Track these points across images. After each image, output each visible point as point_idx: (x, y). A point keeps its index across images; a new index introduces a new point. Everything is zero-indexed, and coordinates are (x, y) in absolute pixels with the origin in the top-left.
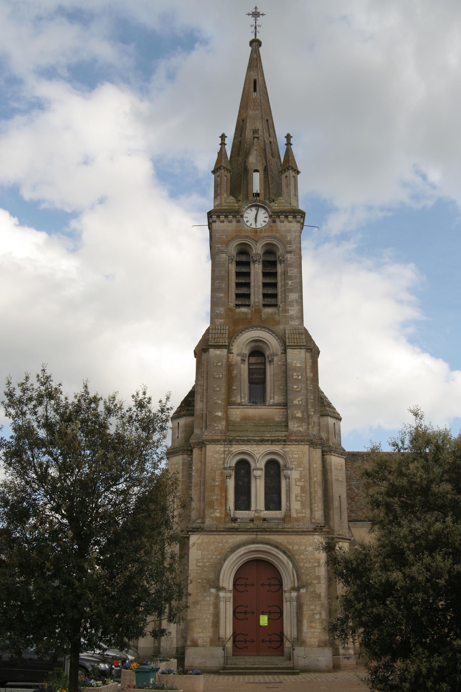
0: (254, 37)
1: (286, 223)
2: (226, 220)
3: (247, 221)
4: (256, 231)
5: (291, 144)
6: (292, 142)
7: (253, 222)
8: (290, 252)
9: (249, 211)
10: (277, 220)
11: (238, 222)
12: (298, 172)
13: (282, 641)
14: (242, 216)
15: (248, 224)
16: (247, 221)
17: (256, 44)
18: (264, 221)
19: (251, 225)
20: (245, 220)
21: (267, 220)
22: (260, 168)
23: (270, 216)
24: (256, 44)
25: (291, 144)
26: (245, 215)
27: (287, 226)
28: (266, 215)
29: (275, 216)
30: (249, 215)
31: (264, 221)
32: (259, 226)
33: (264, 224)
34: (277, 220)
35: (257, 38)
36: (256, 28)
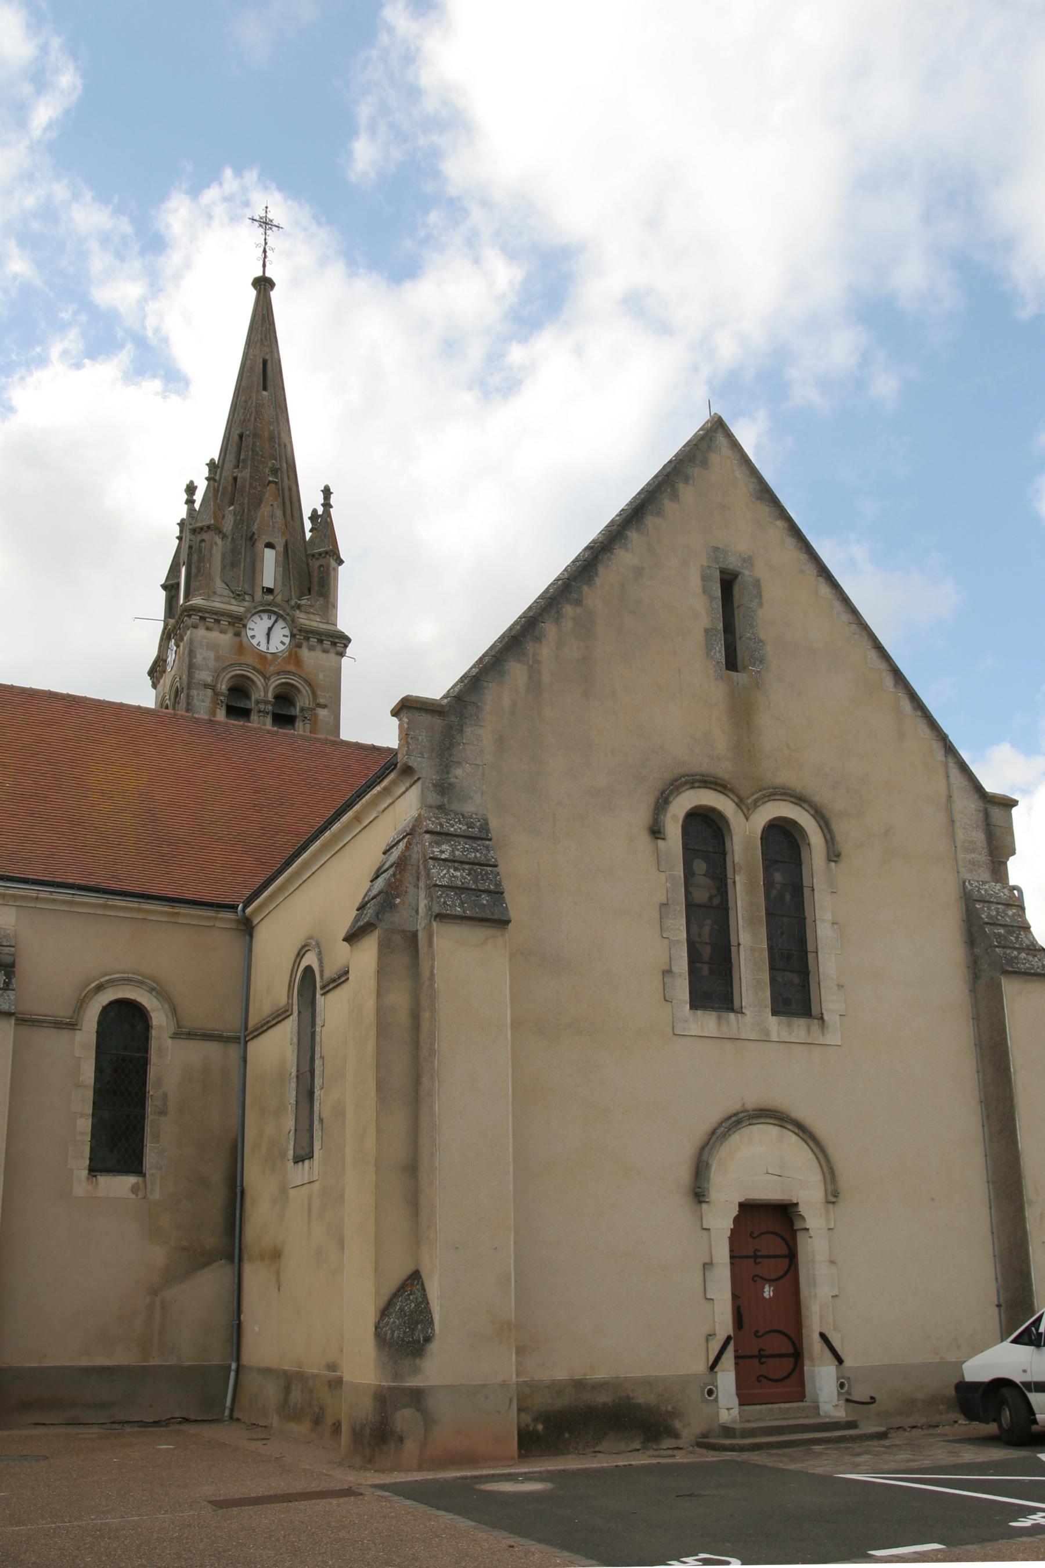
0: (260, 274)
1: (318, 653)
2: (319, 647)
3: (253, 637)
4: (262, 657)
5: (331, 507)
6: (332, 502)
7: (264, 641)
8: (324, 707)
9: (256, 618)
10: (305, 644)
11: (238, 634)
12: (341, 562)
13: (797, 1355)
14: (245, 626)
15: (254, 642)
16: (253, 637)
17: (263, 285)
18: (282, 643)
19: (258, 644)
20: (250, 633)
21: (287, 640)
22: (279, 541)
23: (293, 636)
24: (263, 285)
25: (331, 507)
26: (250, 625)
27: (313, 658)
28: (287, 632)
29: (301, 636)
30: (258, 628)
31: (282, 643)
32: (272, 650)
33: (282, 647)
34: (305, 644)
35: (267, 275)
36: (265, 251)
